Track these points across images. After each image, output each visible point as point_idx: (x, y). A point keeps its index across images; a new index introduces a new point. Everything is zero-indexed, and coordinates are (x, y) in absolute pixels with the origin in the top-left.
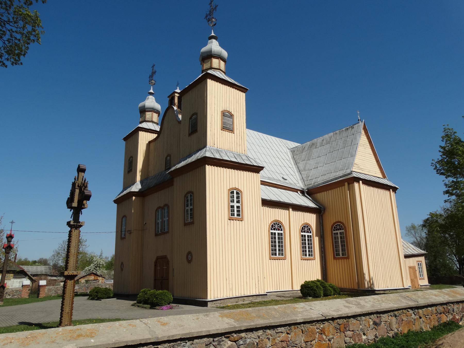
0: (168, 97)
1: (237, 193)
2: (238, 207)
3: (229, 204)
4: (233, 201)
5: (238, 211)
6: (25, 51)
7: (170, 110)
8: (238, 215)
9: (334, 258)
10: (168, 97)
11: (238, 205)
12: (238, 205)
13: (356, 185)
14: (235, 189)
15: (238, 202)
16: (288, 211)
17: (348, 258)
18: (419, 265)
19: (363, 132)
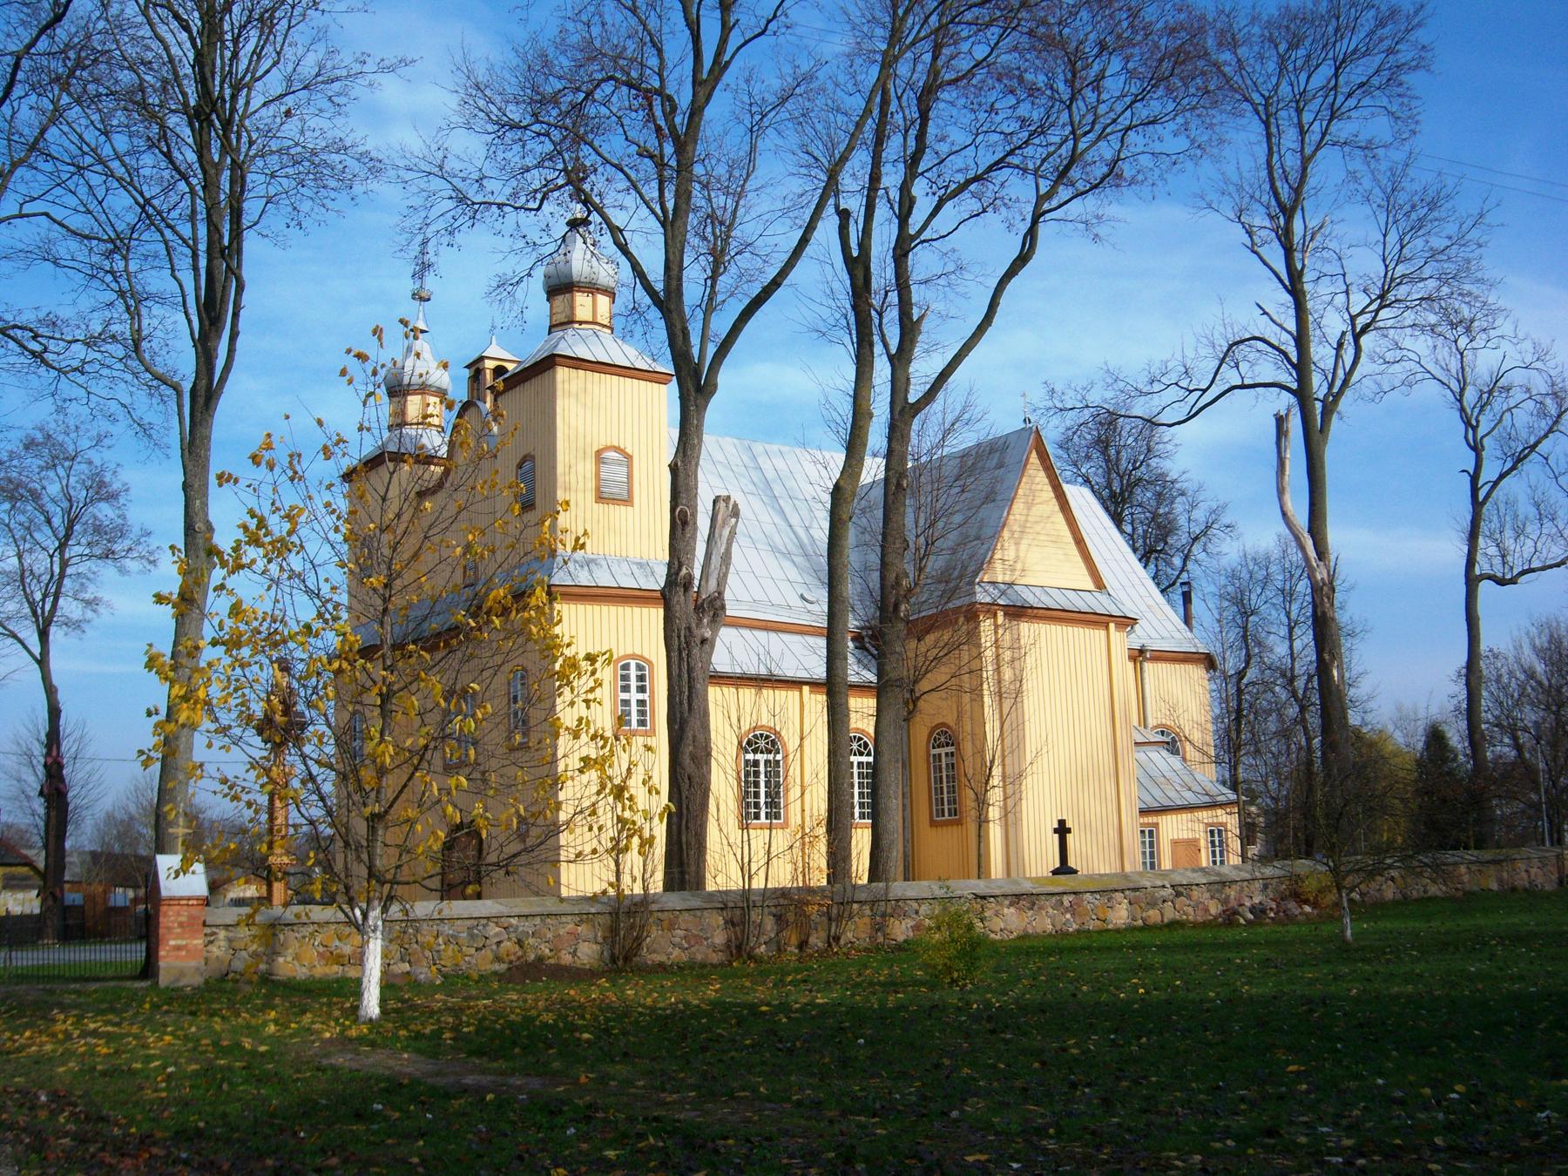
0: (468, 367)
1: (639, 667)
2: (641, 703)
3: (616, 696)
4: (626, 689)
5: (642, 713)
6: (330, 663)
7: (472, 410)
8: (642, 723)
9: (933, 824)
10: (468, 367)
11: (641, 696)
12: (641, 696)
13: (986, 626)
14: (633, 656)
15: (641, 689)
16: (1103, 633)
17: (959, 823)
18: (1216, 834)
19: (1034, 457)
